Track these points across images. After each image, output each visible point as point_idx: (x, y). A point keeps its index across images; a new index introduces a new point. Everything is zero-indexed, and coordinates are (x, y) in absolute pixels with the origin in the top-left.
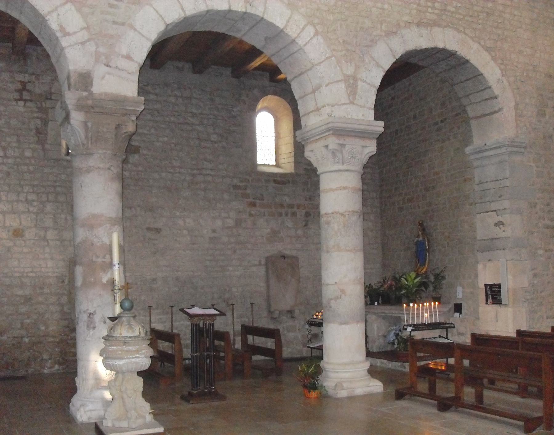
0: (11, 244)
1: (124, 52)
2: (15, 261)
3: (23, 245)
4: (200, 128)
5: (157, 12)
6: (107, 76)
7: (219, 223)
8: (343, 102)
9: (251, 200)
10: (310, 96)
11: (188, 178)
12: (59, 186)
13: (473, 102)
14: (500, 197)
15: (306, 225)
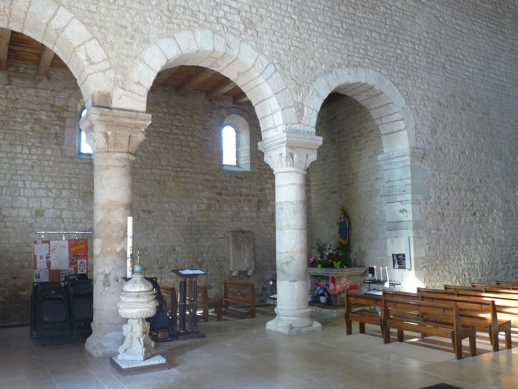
0: (33, 221)
1: (136, 79)
4: (182, 137)
5: (161, 49)
6: (123, 97)
7: (195, 206)
8: (294, 121)
9: (218, 190)
10: (270, 117)
11: (173, 174)
12: (73, 177)
13: (384, 122)
14: (404, 191)
15: (258, 209)
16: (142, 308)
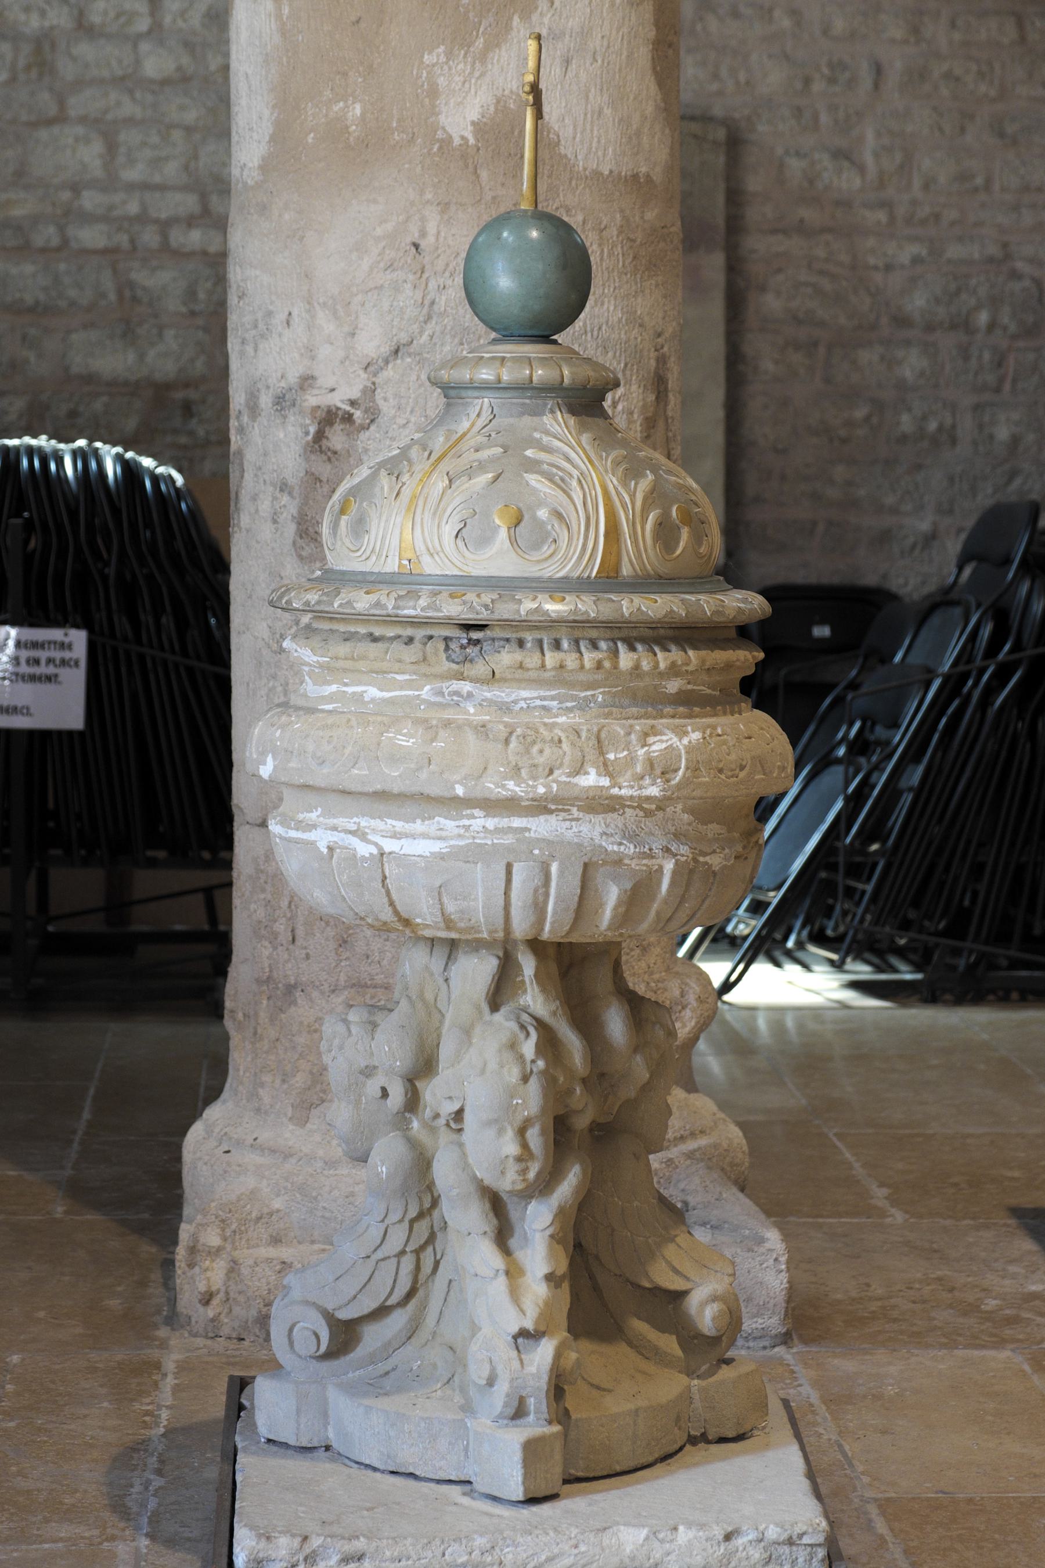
2: (87, 141)
3: (143, 25)
16: (509, 805)
